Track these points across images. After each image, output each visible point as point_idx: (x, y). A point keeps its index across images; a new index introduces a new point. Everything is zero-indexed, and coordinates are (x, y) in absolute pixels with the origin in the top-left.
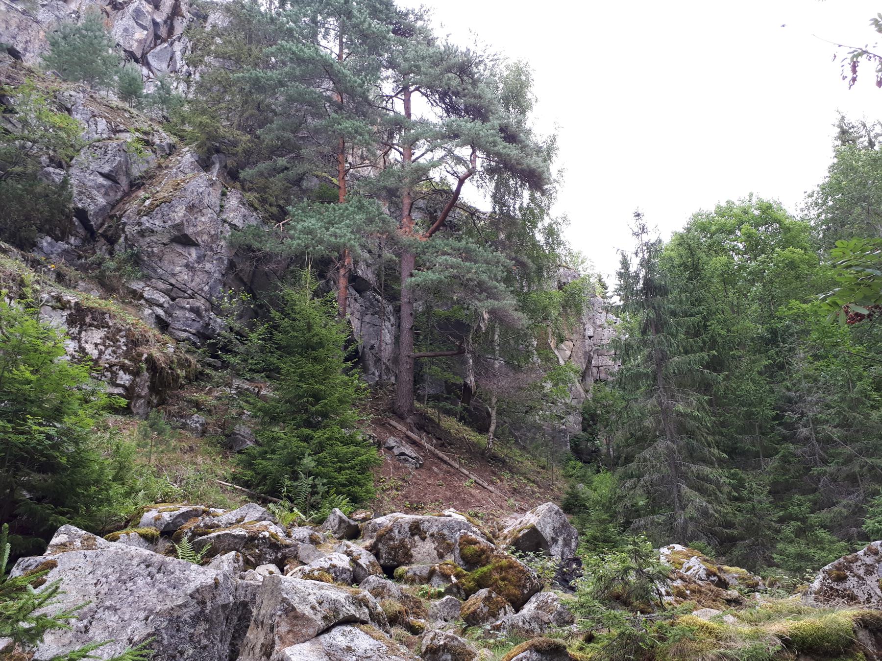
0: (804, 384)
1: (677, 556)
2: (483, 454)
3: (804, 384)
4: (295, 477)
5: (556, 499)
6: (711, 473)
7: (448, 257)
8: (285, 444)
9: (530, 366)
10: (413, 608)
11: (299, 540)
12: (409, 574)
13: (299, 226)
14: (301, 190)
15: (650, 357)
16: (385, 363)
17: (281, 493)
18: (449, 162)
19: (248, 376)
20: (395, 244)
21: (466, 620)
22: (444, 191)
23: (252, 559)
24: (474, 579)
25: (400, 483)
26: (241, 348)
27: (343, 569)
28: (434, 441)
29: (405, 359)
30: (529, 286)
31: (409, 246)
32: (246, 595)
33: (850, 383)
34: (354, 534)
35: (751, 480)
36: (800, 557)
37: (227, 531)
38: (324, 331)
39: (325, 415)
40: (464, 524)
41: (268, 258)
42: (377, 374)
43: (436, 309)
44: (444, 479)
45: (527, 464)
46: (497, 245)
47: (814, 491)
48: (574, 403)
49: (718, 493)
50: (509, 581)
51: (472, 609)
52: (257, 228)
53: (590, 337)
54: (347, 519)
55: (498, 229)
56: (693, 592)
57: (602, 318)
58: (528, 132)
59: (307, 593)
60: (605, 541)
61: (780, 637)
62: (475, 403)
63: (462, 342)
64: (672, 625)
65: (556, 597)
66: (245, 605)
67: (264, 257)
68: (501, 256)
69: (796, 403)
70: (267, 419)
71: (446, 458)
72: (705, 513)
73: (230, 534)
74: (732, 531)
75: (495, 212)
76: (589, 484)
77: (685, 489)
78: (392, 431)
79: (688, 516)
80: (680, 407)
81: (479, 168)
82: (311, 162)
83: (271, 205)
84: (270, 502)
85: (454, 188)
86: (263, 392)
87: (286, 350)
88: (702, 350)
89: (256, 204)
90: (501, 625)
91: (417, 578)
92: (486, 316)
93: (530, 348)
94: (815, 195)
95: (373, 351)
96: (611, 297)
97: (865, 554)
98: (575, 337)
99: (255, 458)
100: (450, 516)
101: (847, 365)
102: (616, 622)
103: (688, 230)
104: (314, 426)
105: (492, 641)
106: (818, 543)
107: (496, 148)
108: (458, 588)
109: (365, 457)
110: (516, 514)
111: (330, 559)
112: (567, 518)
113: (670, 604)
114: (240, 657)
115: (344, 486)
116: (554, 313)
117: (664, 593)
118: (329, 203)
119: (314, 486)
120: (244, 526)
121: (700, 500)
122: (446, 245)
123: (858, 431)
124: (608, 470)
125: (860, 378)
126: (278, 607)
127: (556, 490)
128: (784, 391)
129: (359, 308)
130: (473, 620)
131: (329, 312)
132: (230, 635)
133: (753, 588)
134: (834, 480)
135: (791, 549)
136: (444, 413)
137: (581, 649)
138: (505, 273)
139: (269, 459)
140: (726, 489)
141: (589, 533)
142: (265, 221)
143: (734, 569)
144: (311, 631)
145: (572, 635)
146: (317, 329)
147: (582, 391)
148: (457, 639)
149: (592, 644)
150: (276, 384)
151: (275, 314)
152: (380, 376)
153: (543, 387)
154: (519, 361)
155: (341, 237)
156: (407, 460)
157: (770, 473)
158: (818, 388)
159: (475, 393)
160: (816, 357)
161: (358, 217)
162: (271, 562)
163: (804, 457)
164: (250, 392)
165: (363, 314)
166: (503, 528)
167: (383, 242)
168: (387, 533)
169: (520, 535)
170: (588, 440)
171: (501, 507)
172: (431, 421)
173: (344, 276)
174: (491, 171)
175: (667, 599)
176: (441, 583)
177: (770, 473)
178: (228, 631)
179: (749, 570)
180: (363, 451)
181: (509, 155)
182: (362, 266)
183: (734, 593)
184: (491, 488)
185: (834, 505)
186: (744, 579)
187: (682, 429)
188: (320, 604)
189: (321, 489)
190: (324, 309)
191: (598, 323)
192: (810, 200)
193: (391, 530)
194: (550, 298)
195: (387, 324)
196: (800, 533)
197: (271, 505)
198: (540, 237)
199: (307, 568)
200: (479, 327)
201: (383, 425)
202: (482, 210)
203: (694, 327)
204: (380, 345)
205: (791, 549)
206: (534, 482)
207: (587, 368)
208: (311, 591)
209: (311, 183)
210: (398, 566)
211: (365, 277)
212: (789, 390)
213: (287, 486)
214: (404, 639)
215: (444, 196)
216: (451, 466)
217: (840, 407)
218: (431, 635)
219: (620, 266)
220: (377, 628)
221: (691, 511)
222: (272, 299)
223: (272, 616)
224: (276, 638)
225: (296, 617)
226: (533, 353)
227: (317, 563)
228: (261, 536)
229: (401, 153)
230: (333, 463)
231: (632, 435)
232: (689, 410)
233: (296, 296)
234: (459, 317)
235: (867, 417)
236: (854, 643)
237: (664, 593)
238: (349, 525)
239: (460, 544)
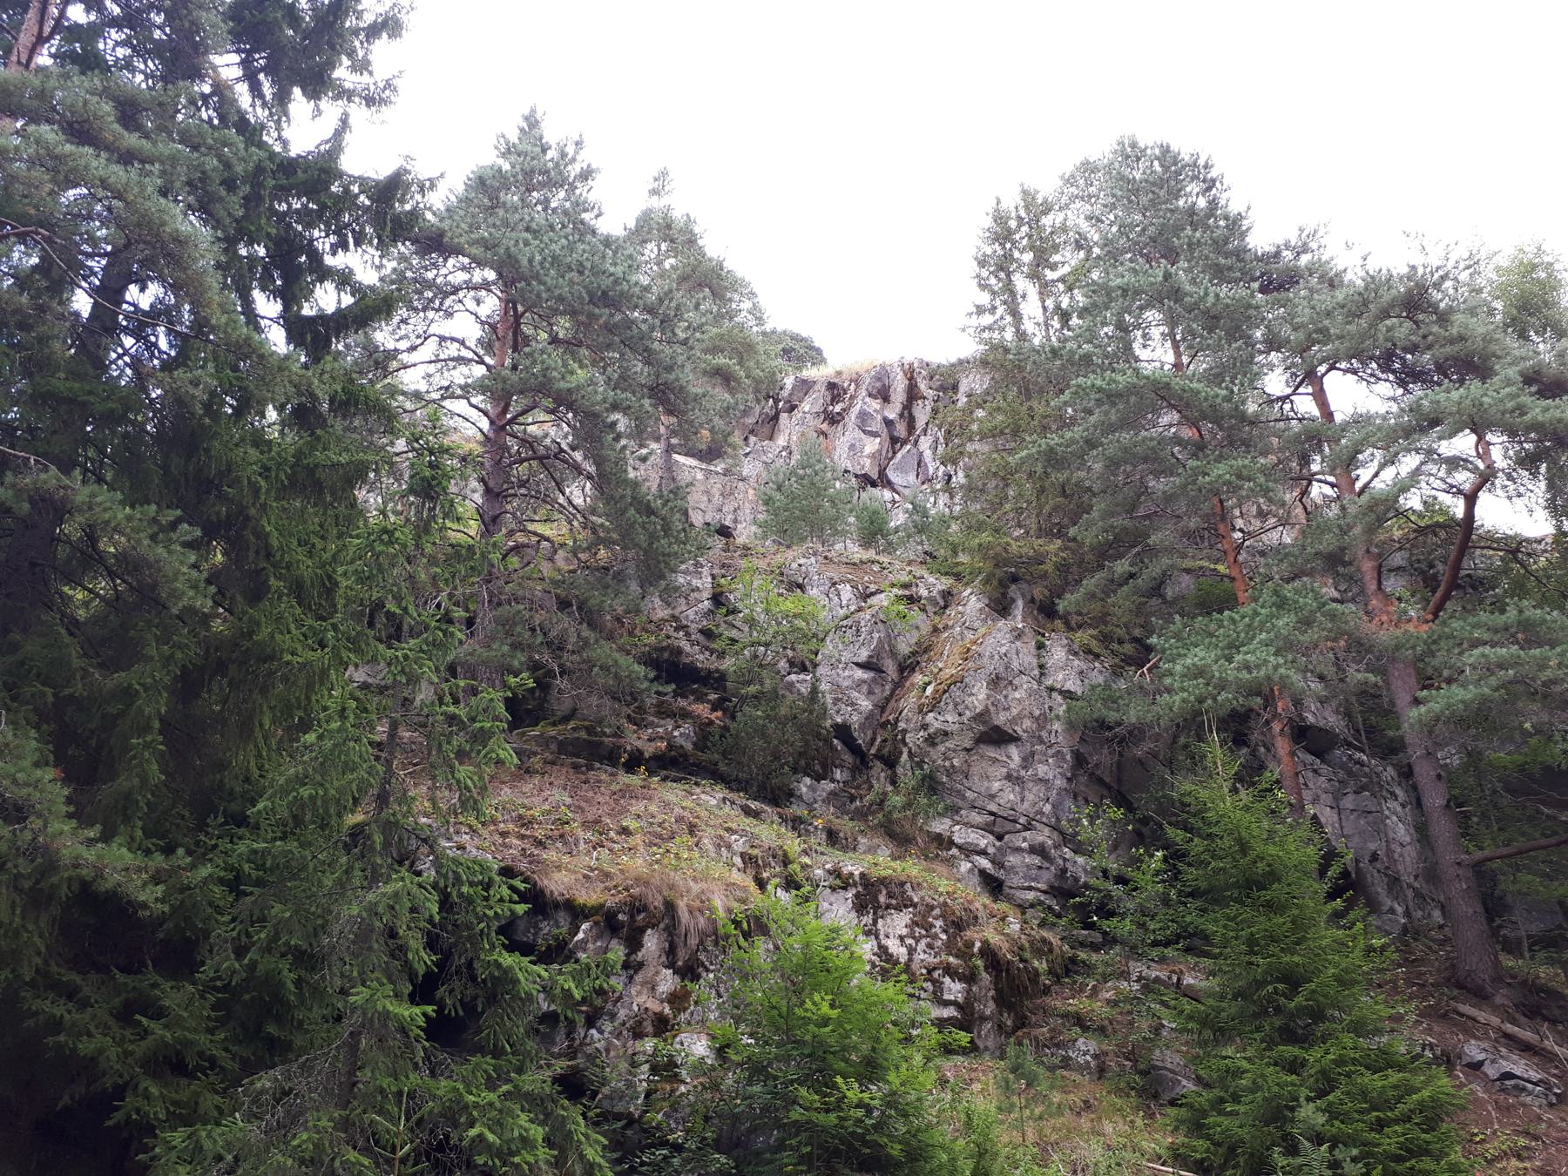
7: (1487, 650)
8: (1254, 1082)
22: (1438, 525)
25: (1522, 1142)
29: (1453, 871)
31: (1397, 647)
38: (1272, 850)
39: (1318, 1015)
41: (1136, 733)
42: (1399, 910)
52: (1107, 687)
67: (1130, 733)
70: (1208, 1034)
78: (1470, 1028)
83: (1121, 642)
86: (1188, 980)
87: (1208, 896)
89: (1094, 645)
95: (1378, 865)
104: (1303, 1040)
107: (1527, 418)
115: (1398, 1159)
139: (1231, 1114)
142: (1117, 672)
146: (1258, 847)
151: (1176, 835)
152: (1407, 914)
155: (1258, 667)
156: (1524, 1089)
165: (1337, 797)
204: (1389, 852)
211: (1322, 723)
215: (1443, 534)
233: (1203, 794)
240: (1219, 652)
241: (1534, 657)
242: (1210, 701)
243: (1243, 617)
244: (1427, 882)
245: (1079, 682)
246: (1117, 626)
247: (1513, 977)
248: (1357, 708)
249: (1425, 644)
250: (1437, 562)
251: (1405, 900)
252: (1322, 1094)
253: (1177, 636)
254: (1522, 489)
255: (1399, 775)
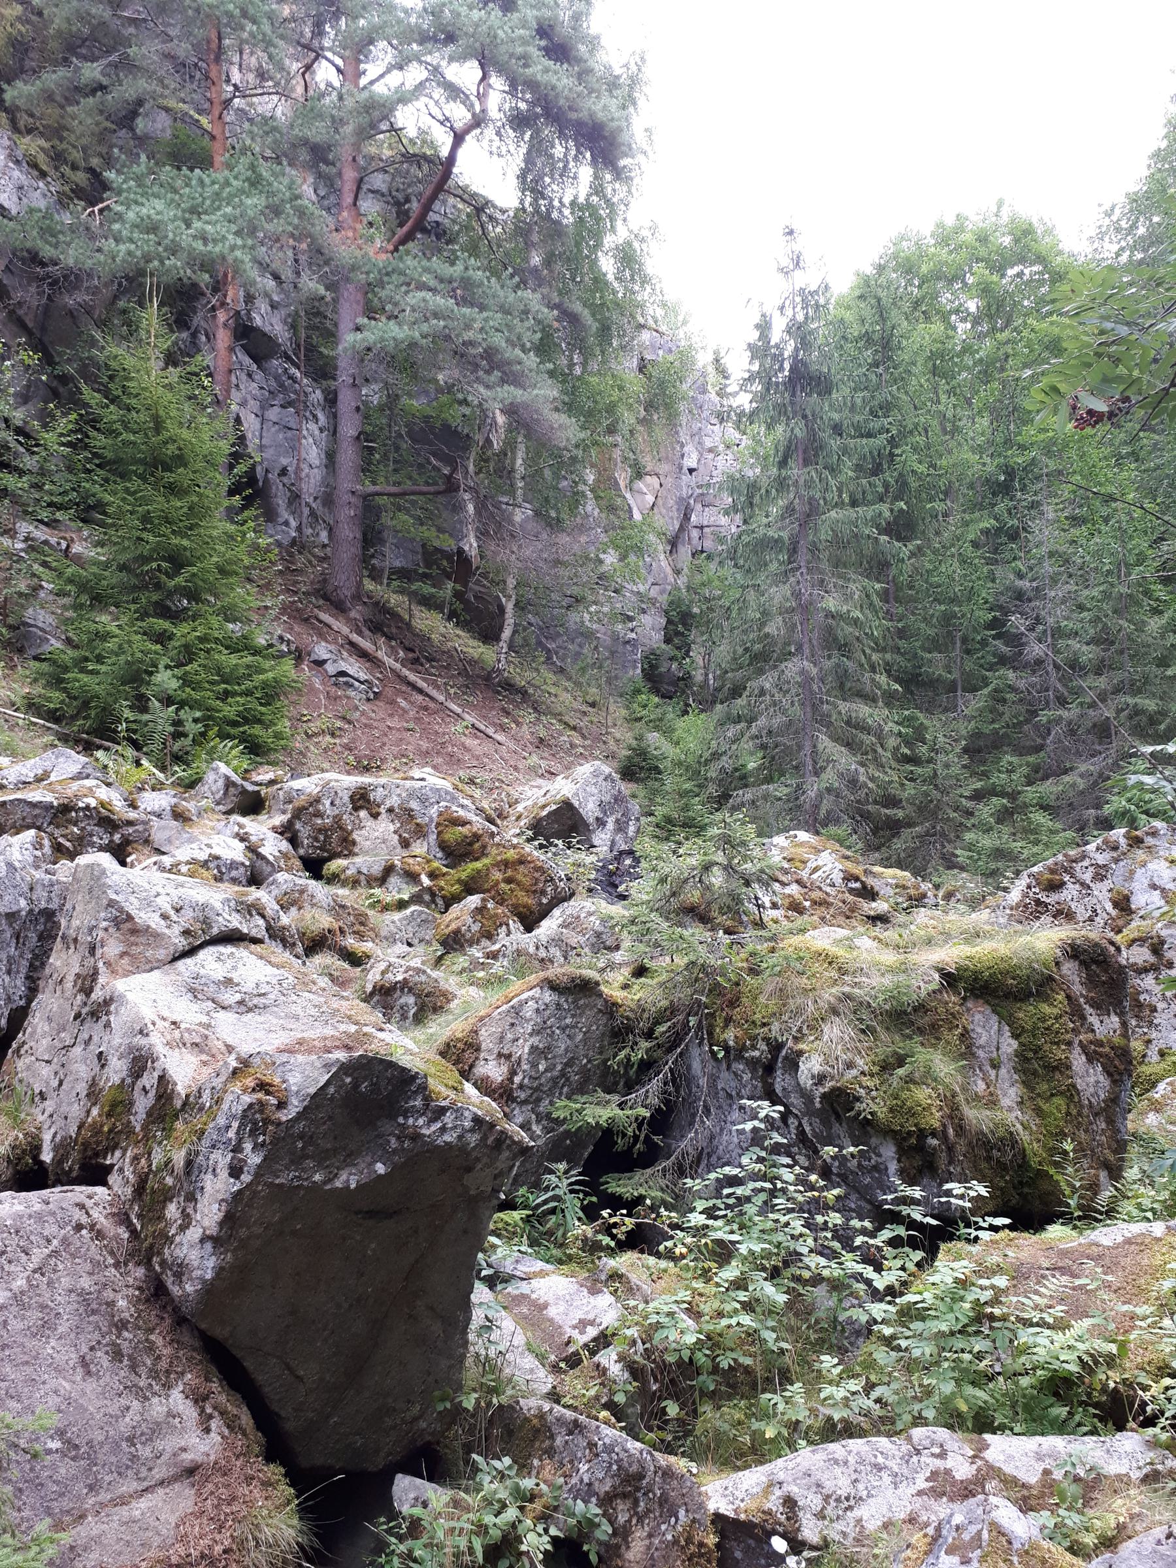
0: (1049, 568)
1: (800, 850)
2: (488, 678)
3: (1049, 568)
4: (141, 704)
5: (609, 757)
6: (871, 715)
7: (428, 295)
8: (120, 647)
9: (579, 520)
10: (353, 925)
11: (153, 813)
12: (349, 872)
13: (131, 215)
14: (135, 137)
15: (789, 510)
16: (307, 504)
17: (115, 731)
18: (436, 96)
19: (44, 515)
20: (327, 263)
21: (444, 943)
22: (425, 157)
23: (68, 844)
24: (459, 881)
25: (339, 724)
26: (29, 462)
27: (233, 862)
28: (401, 654)
29: (347, 497)
30: (584, 364)
31: (353, 268)
32: (50, 899)
33: (1122, 566)
34: (252, 805)
35: (936, 727)
36: (999, 853)
37: (19, 795)
38: (185, 434)
39: (194, 596)
40: (447, 792)
41: (72, 279)
42: (293, 524)
43: (405, 400)
44: (418, 720)
45: (565, 698)
46: (525, 277)
47: (1039, 749)
48: (654, 592)
49: (880, 750)
50: (518, 884)
51: (453, 926)
52: (47, 216)
53: (691, 471)
54: (239, 781)
55: (529, 245)
56: (814, 903)
57: (715, 435)
58: (594, 43)
59: (154, 893)
60: (685, 825)
61: (940, 970)
62: (477, 588)
63: (454, 470)
64: (773, 950)
65: (593, 908)
66: (49, 915)
67: (65, 277)
68: (532, 298)
69: (1030, 600)
70: (85, 599)
71: (421, 684)
72: (853, 783)
73: (25, 801)
74: (895, 811)
75: (524, 210)
76: (668, 732)
77: (825, 742)
78: (323, 632)
79: (824, 785)
80: (831, 603)
81: (493, 112)
82: (150, 75)
83: (74, 167)
84: (99, 747)
85: (444, 152)
86: (76, 549)
87: (115, 468)
88: (881, 500)
89: (42, 160)
90: (499, 951)
91: (362, 878)
92: (501, 419)
93: (581, 487)
94: (1117, 212)
95: (285, 479)
96: (735, 394)
97: (1098, 849)
98: (664, 468)
99: (66, 669)
100: (422, 779)
101: (1123, 536)
102: (680, 945)
103: (881, 269)
104: (175, 616)
105: (481, 974)
106: (1030, 832)
107: (528, 71)
108: (433, 895)
109: (270, 675)
110: (540, 781)
111: (209, 846)
112: (626, 788)
113: (776, 922)
114: (40, 996)
115: (235, 724)
116: (628, 418)
117: (768, 904)
118: (192, 169)
119: (177, 723)
120: (50, 788)
121: (846, 760)
122: (426, 270)
123: (1122, 652)
124: (702, 711)
125: (1141, 560)
126: (103, 915)
127: (612, 742)
128: (1012, 577)
129: (256, 392)
130: (453, 942)
131: (195, 397)
132: (25, 963)
133: (918, 900)
134: (1072, 732)
135: (987, 842)
136: (420, 603)
137: (625, 987)
138: (539, 335)
139: (92, 672)
140: (892, 742)
141: (660, 811)
142: (63, 201)
143: (891, 871)
144: (162, 954)
145: (611, 966)
146: (172, 429)
147: (669, 570)
148: (424, 972)
149: (642, 980)
150: (98, 533)
151: (90, 396)
152: (299, 529)
153: (601, 562)
154: (558, 511)
155: (215, 241)
156: (352, 686)
157: (970, 719)
158: (1070, 576)
159: (478, 568)
160: (1076, 521)
161: (249, 202)
162: (101, 849)
163: (1029, 693)
164: (51, 546)
165: (265, 405)
166: (517, 802)
167: (303, 258)
168: (311, 804)
169: (544, 813)
170: (672, 659)
171: (516, 769)
172: (395, 616)
173: (225, 325)
174: (519, 121)
175: (775, 913)
176: (404, 886)
177: (970, 719)
178: (21, 956)
179: (915, 874)
180: (267, 664)
181: (553, 88)
182: (263, 306)
183: (880, 906)
184: (500, 737)
185: (1066, 772)
186: (904, 887)
187: (833, 643)
188: (177, 911)
189: (192, 728)
190: (185, 389)
191: (708, 443)
192: (1107, 221)
193: (318, 800)
194: (621, 388)
195: (312, 426)
196: (1004, 816)
197: (100, 754)
198: (607, 265)
199: (167, 860)
200: (488, 441)
201: (306, 620)
202: (500, 203)
203: (873, 458)
204: (298, 469)
205: (987, 842)
206: (574, 728)
207: (682, 528)
208: (161, 890)
209: (155, 124)
210: (329, 859)
211: (267, 329)
212: (1021, 576)
213: (127, 721)
214: (336, 974)
215: (425, 167)
216: (432, 698)
217: (1100, 609)
218: (382, 966)
219: (757, 334)
220: (279, 949)
221: (829, 777)
222: (85, 366)
223: (91, 930)
224: (100, 964)
225: (134, 931)
226: (584, 496)
227: (183, 853)
228: (81, 805)
229: (339, 70)
230: (212, 683)
231: (746, 650)
232: (845, 608)
233: (130, 362)
234: (451, 421)
235: (1140, 627)
236: (1053, 980)
237: (768, 904)
238: (244, 792)
239: (438, 825)
240: (180, 214)
241: (464, 316)
242: (156, 263)
243: (213, 183)
244: (324, 505)
245: (15, 199)
246: (74, 147)
247: (369, 597)
248: (303, 322)
249: (379, 272)
250: (414, 199)
251: (301, 516)
252: (180, 665)
253: (139, 179)
254: (504, 149)
255: (326, 399)
